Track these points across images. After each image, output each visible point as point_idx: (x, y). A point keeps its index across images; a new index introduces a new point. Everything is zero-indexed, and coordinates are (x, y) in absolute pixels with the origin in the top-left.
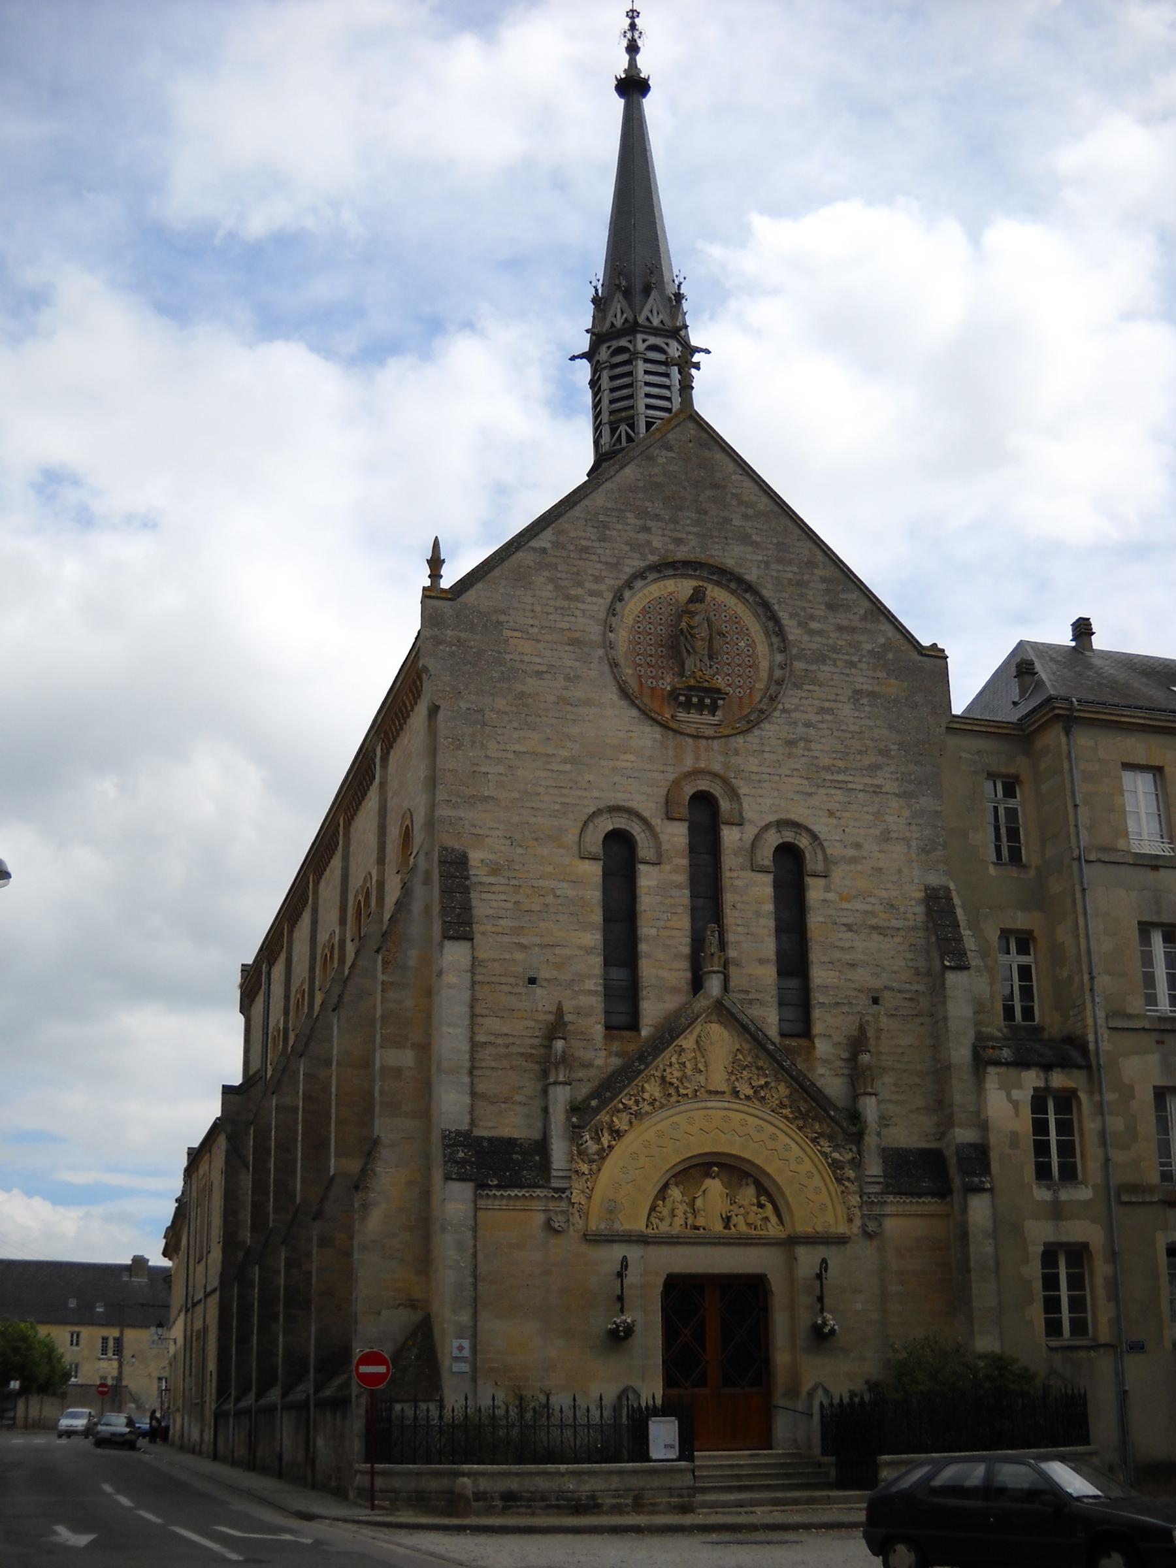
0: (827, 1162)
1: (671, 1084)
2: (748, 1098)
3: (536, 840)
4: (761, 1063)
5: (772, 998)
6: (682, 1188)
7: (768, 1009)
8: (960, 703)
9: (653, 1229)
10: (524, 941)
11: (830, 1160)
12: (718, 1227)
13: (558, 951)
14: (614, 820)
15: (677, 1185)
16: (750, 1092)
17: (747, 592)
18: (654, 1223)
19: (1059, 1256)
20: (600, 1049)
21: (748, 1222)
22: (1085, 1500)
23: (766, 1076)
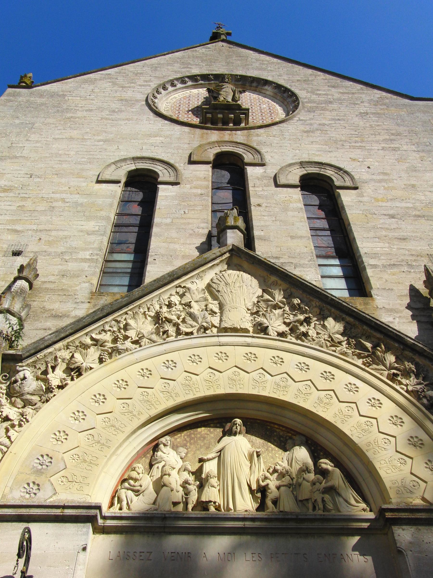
0: (423, 404)
1: (169, 321)
2: (282, 335)
3: (57, 174)
4: (296, 301)
5: (309, 262)
6: (183, 451)
7: (305, 269)
8: (360, 537)
9: (121, 509)
10: (18, 227)
11: (425, 401)
12: (135, 465)
13: (54, 233)
14: (137, 164)
15: (175, 448)
16: (284, 328)
17: (265, 86)
18: (123, 497)
19: (118, 535)
20: (82, 302)
21: (300, 498)
22: (46, 338)
23: (305, 312)
